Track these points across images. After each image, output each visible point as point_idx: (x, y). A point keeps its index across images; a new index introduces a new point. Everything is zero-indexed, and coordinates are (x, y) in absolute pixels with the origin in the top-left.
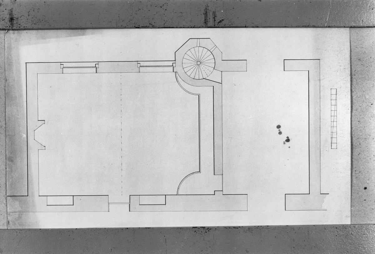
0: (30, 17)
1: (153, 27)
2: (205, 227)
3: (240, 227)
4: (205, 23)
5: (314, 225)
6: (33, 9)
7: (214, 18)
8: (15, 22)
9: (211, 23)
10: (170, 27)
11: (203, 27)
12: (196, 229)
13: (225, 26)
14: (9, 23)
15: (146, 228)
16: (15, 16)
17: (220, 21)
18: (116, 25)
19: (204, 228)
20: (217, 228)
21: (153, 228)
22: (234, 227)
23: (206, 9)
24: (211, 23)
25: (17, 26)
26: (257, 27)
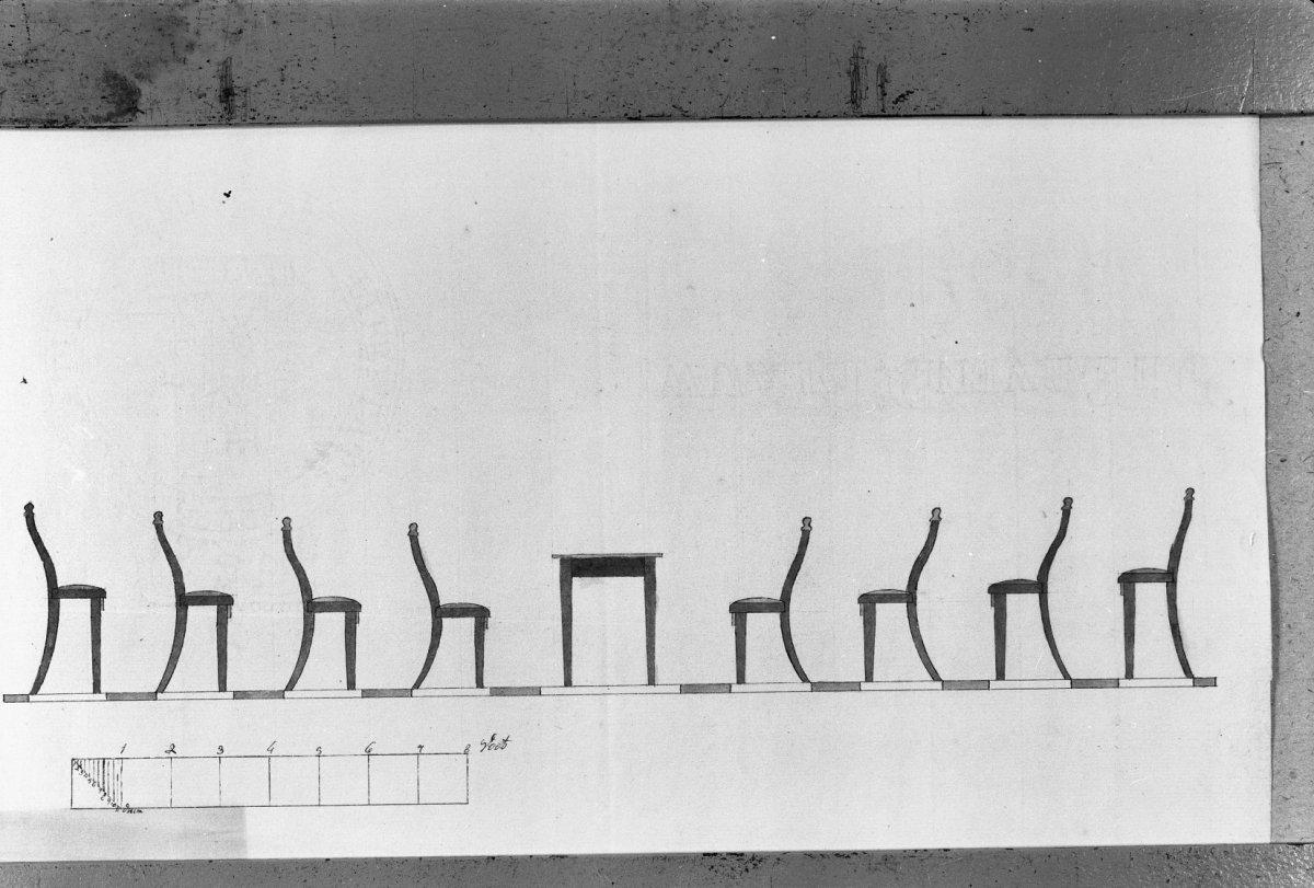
0: (288, 85)
1: (686, 116)
2: (742, 854)
3: (855, 853)
4: (853, 102)
5: (1096, 848)
6: (296, 62)
7: (882, 86)
8: (238, 102)
9: (871, 101)
10: (738, 118)
11: (845, 116)
12: (717, 861)
13: (915, 113)
14: (219, 107)
15: (553, 857)
16: (237, 83)
17: (902, 96)
18: (565, 112)
19: (739, 855)
20: (781, 858)
21: (575, 858)
22: (838, 855)
23: (856, 56)
24: (871, 101)
25: (245, 115)
26: (1022, 115)
